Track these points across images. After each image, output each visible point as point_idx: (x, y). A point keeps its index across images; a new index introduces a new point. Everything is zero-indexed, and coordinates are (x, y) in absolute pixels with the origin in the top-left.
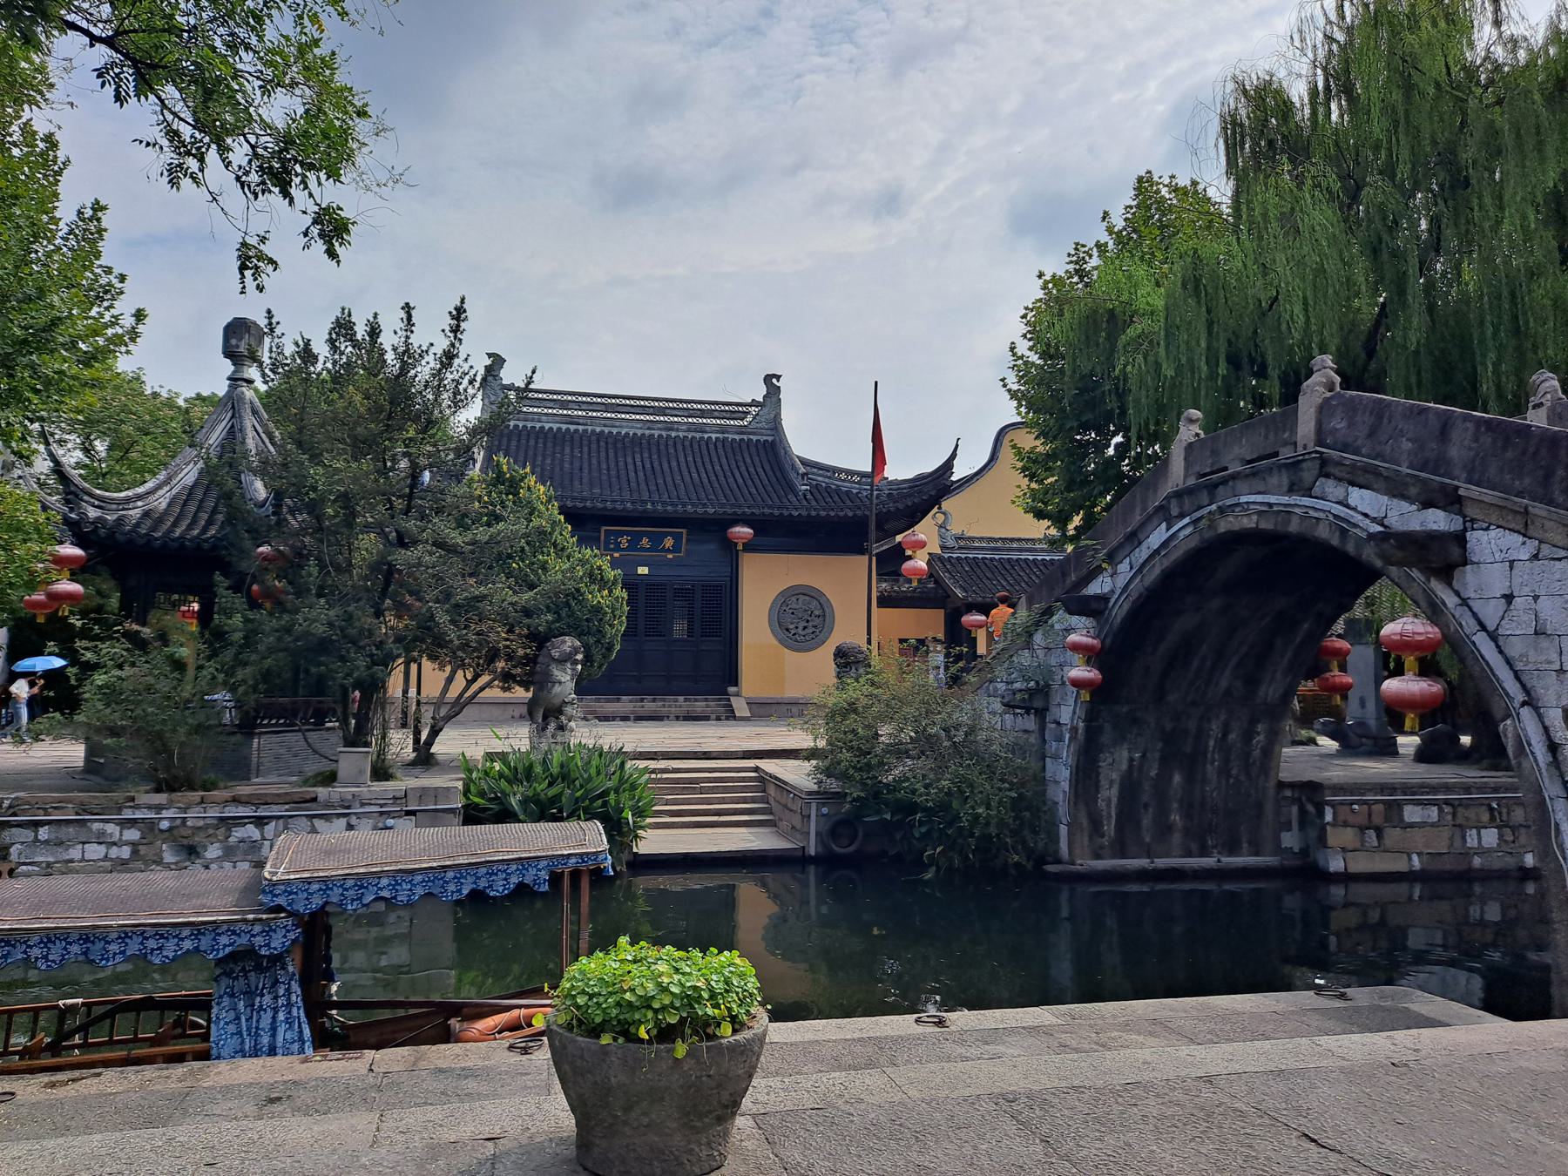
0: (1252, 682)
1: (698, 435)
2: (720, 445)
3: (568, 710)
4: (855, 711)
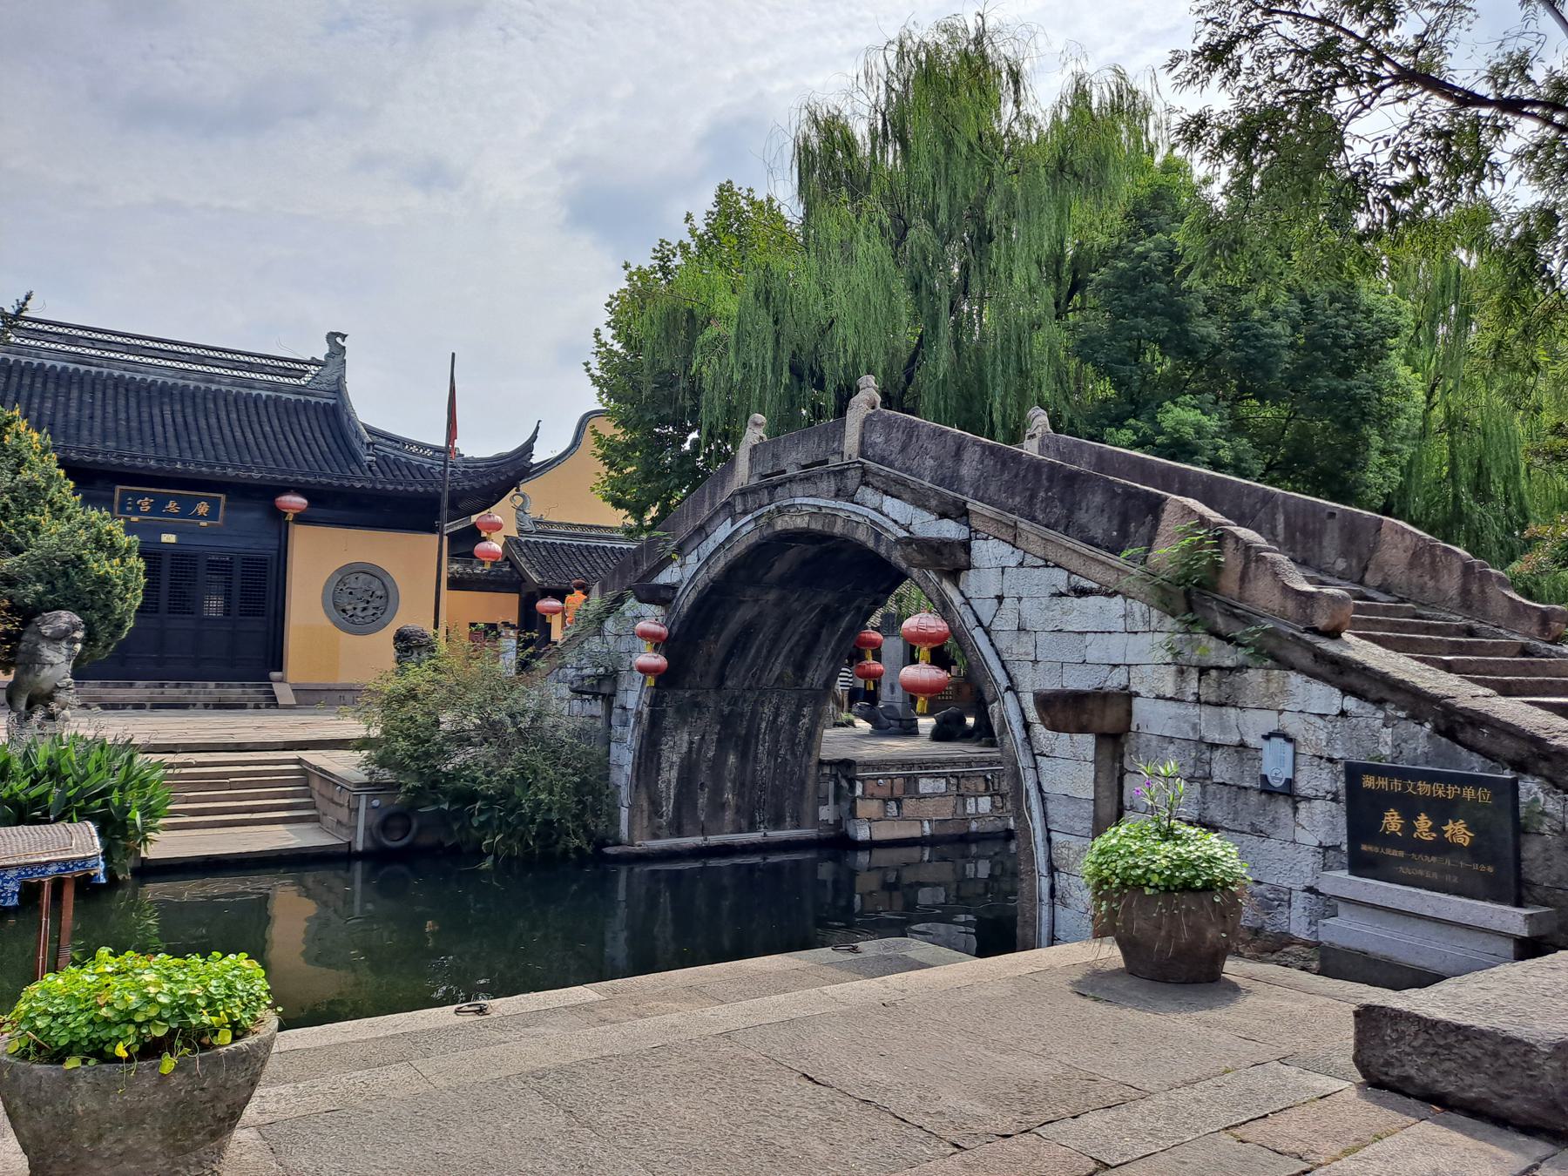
0: (801, 668)
1: (244, 391)
2: (271, 404)
3: (62, 696)
4: (415, 698)
